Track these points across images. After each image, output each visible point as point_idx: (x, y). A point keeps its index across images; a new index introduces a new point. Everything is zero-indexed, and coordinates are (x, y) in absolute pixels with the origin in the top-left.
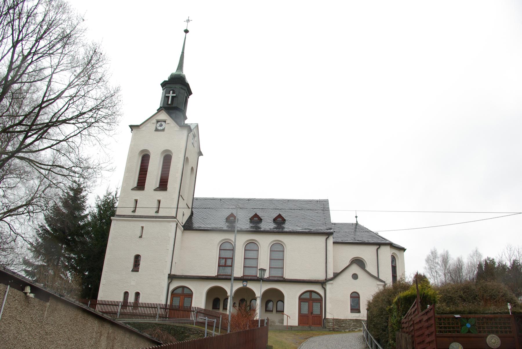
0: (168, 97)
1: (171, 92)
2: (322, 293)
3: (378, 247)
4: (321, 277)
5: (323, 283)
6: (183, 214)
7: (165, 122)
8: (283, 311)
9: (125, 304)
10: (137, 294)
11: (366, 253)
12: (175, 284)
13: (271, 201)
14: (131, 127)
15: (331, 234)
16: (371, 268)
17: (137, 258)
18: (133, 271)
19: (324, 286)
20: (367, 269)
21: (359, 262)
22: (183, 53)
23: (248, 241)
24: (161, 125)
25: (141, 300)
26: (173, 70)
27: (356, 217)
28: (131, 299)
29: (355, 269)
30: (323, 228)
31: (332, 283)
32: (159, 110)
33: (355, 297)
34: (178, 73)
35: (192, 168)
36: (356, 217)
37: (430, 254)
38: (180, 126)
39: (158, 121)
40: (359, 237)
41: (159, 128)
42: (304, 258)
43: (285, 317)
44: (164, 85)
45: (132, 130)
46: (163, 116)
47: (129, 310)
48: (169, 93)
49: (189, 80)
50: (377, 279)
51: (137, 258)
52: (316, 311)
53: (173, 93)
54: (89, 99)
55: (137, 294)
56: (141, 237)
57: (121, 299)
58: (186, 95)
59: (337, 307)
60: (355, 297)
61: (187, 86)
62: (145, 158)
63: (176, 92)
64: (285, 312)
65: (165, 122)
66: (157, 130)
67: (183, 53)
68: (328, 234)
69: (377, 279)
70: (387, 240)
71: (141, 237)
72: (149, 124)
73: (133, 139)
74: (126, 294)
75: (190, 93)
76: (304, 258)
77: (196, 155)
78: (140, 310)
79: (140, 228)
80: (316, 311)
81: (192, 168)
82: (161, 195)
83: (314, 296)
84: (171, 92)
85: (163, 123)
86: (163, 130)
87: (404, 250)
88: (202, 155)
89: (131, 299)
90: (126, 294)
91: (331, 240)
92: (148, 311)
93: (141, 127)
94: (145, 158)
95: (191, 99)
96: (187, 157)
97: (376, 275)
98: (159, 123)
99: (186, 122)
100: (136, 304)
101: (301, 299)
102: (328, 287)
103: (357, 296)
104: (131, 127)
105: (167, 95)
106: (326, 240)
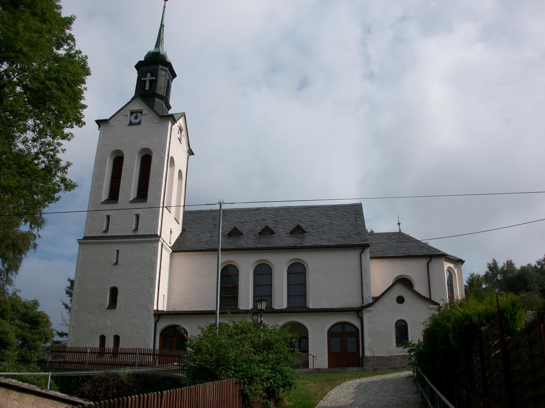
0: (145, 81)
1: (149, 75)
2: (357, 324)
3: (428, 260)
4: (355, 303)
5: (358, 312)
6: (171, 232)
7: (141, 112)
8: (308, 351)
9: (102, 351)
10: (117, 339)
11: (413, 270)
12: (163, 324)
13: (287, 209)
14: (98, 122)
15: (367, 246)
16: (420, 287)
17: (114, 292)
18: (109, 308)
19: (360, 315)
20: (416, 288)
21: (404, 282)
22: (162, 26)
23: (261, 260)
24: (136, 118)
25: (122, 345)
26: (152, 48)
27: (399, 224)
28: (110, 344)
29: (400, 291)
30: (356, 241)
31: (370, 310)
32: (133, 99)
33: (402, 329)
34: (157, 50)
35: (180, 172)
36: (399, 224)
37: (488, 270)
38: (161, 117)
39: (132, 113)
40: (400, 247)
41: (134, 121)
42: (330, 281)
43: (310, 358)
44: (139, 66)
45: (99, 127)
46: (138, 106)
47: (107, 358)
48: (146, 77)
49: (170, 58)
50: (429, 300)
51: (114, 292)
52: (351, 348)
53: (152, 76)
54: (472, 310)
55: (117, 339)
56: (116, 263)
57: (97, 345)
58: (168, 77)
59: (378, 340)
60: (402, 329)
61: (169, 65)
62: (118, 161)
63: (154, 71)
64: (310, 352)
65: (141, 112)
66: (131, 124)
67: (162, 26)
68: (363, 247)
69: (429, 300)
70: (439, 251)
71: (116, 263)
72: (120, 117)
73: (101, 138)
74: (103, 339)
75: (174, 75)
76: (330, 281)
77: (186, 155)
78: (120, 359)
79: (116, 253)
80: (351, 348)
81: (180, 172)
82: (140, 208)
83: (348, 329)
84: (149, 75)
85: (139, 115)
86: (139, 123)
87: (461, 262)
88: (193, 154)
89: (110, 344)
90: (103, 339)
91: (367, 254)
92: (130, 359)
93: (110, 121)
94: (118, 161)
95: (175, 84)
96: (172, 157)
97: (426, 295)
98: (134, 115)
99: (170, 112)
100: (115, 353)
101: (331, 334)
102: (366, 316)
103: (404, 324)
104: (98, 122)
105: (143, 79)
106: (361, 255)
